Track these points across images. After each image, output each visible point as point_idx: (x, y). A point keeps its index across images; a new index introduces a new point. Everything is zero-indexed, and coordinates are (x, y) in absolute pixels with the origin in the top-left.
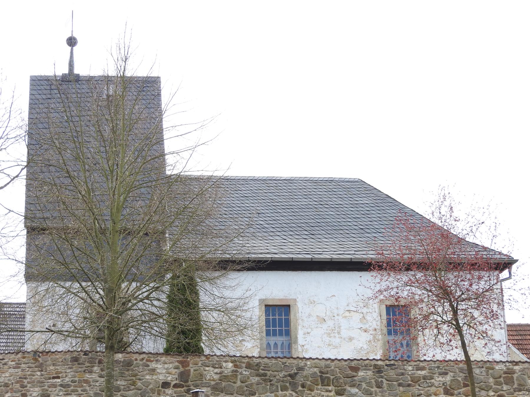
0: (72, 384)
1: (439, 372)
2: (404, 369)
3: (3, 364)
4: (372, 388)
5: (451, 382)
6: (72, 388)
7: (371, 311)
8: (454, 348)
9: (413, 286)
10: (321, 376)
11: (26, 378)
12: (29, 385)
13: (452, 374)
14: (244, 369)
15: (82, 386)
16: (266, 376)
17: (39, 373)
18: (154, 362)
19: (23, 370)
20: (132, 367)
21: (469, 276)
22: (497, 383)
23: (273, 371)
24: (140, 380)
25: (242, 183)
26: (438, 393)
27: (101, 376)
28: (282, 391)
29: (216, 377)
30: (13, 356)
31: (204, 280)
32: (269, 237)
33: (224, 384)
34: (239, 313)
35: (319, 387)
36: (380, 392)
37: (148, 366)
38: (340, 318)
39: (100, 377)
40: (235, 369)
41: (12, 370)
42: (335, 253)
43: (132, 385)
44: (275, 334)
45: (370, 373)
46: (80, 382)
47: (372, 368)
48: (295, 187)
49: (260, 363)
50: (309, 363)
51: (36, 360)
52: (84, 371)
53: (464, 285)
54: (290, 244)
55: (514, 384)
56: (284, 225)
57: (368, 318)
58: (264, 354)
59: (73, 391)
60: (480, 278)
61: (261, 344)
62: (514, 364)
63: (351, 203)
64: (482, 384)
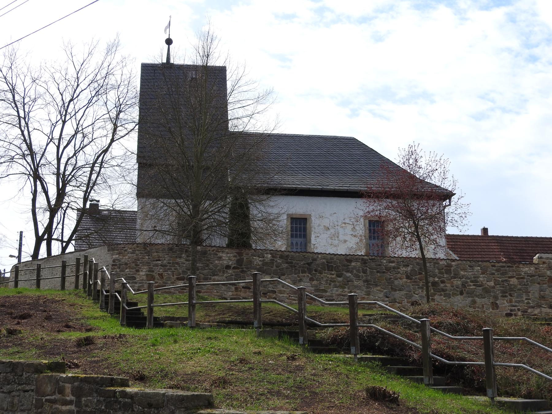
0: (168, 264)
1: (403, 265)
2: (381, 262)
3: (124, 251)
4: (360, 273)
5: (411, 271)
6: (168, 267)
7: (359, 224)
8: (414, 250)
9: (390, 210)
10: (327, 265)
11: (139, 260)
12: (141, 265)
13: (411, 266)
14: (278, 258)
15: (175, 266)
16: (292, 263)
17: (147, 257)
18: (221, 252)
19: (137, 255)
20: (207, 255)
21: (426, 205)
22: (440, 273)
23: (296, 261)
24: (212, 263)
25: (278, 138)
26: (402, 278)
27: (187, 260)
28: (302, 273)
29: (260, 263)
30: (131, 246)
31: (255, 201)
32: (330, 176)
33: (265, 267)
34: (274, 222)
35: (326, 272)
36: (365, 276)
37: (217, 255)
38: (339, 227)
39: (186, 261)
40: (272, 258)
41: (130, 255)
42: (337, 185)
43: (207, 267)
44: (296, 237)
45: (359, 264)
46: (173, 263)
47: (360, 260)
48: (312, 142)
49: (289, 255)
50: (320, 256)
51: (145, 249)
52: (176, 257)
53: (423, 210)
54: (308, 179)
55: (451, 274)
56: (304, 166)
57: (357, 228)
58: (289, 249)
59: (169, 269)
60: (433, 206)
61: (288, 243)
62: (452, 261)
63: (348, 153)
64: (431, 273)
